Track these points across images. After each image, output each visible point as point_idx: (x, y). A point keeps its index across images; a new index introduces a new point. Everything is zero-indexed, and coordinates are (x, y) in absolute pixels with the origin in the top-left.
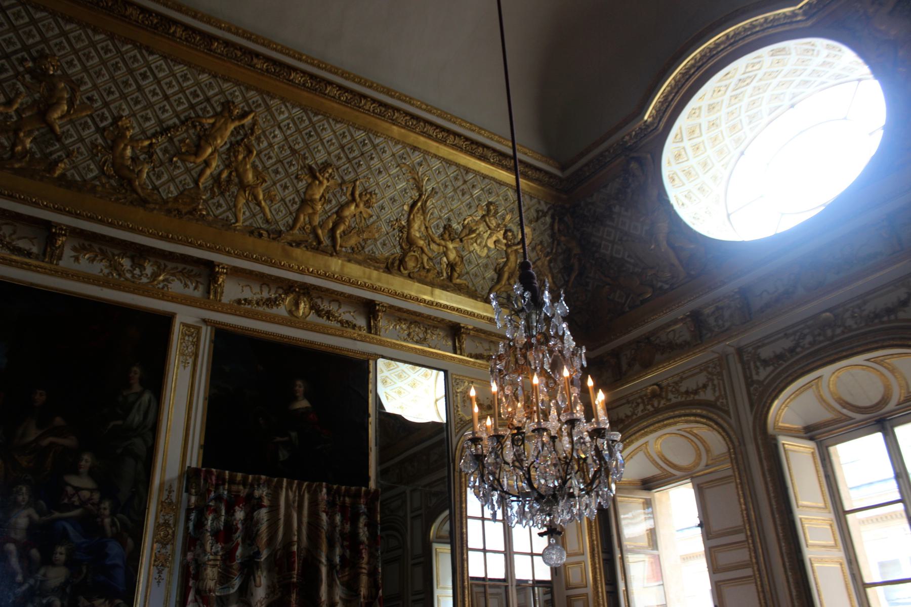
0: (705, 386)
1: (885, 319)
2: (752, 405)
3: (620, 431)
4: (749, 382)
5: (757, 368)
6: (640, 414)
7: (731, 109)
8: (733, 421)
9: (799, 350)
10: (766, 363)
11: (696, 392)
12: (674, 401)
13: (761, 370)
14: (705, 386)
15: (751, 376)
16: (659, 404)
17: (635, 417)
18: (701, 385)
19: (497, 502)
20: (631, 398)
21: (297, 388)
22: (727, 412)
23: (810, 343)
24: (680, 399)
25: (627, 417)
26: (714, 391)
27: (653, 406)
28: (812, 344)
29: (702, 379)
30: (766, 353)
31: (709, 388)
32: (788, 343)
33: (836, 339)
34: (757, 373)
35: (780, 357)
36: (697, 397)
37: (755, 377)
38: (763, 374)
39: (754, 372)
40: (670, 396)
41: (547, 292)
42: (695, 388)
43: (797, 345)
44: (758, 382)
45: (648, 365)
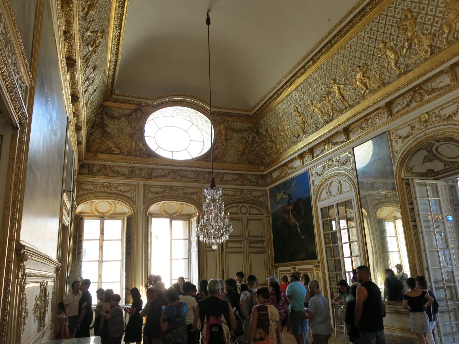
0: (128, 191)
1: (189, 195)
2: (144, 204)
3: (212, 248)
4: (145, 196)
5: (149, 193)
6: (97, 191)
7: (435, 143)
8: (136, 206)
9: (163, 193)
10: (152, 193)
11: (124, 192)
12: (114, 191)
13: (150, 194)
14: (128, 191)
15: (146, 194)
16: (107, 190)
17: (94, 191)
18: (126, 190)
19: (215, 280)
20: (94, 183)
21: (237, 284)
22: (134, 202)
23: (167, 193)
24: (116, 192)
25: (91, 190)
26: (131, 194)
27: (104, 190)
28: (168, 193)
29: (127, 188)
30: (153, 190)
31: (196, 194)
32: (231, 193)
33: (175, 195)
34: (148, 195)
35: (157, 193)
36: (124, 194)
37: (147, 195)
38: (150, 196)
39: (147, 194)
40: (113, 189)
41: (416, 281)
42: (124, 190)
43: (163, 192)
44: (147, 197)
45: (106, 175)
